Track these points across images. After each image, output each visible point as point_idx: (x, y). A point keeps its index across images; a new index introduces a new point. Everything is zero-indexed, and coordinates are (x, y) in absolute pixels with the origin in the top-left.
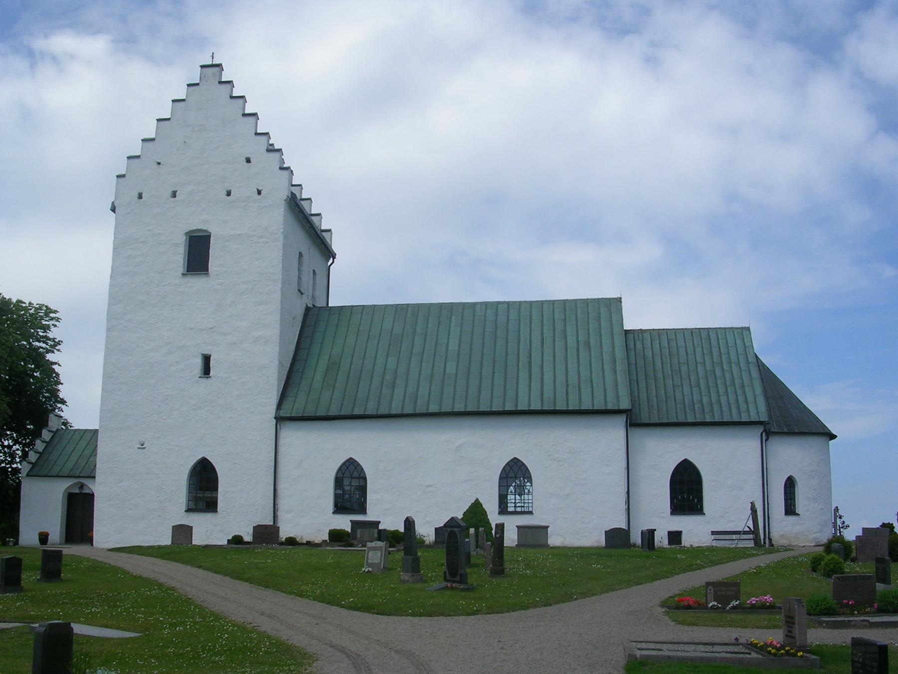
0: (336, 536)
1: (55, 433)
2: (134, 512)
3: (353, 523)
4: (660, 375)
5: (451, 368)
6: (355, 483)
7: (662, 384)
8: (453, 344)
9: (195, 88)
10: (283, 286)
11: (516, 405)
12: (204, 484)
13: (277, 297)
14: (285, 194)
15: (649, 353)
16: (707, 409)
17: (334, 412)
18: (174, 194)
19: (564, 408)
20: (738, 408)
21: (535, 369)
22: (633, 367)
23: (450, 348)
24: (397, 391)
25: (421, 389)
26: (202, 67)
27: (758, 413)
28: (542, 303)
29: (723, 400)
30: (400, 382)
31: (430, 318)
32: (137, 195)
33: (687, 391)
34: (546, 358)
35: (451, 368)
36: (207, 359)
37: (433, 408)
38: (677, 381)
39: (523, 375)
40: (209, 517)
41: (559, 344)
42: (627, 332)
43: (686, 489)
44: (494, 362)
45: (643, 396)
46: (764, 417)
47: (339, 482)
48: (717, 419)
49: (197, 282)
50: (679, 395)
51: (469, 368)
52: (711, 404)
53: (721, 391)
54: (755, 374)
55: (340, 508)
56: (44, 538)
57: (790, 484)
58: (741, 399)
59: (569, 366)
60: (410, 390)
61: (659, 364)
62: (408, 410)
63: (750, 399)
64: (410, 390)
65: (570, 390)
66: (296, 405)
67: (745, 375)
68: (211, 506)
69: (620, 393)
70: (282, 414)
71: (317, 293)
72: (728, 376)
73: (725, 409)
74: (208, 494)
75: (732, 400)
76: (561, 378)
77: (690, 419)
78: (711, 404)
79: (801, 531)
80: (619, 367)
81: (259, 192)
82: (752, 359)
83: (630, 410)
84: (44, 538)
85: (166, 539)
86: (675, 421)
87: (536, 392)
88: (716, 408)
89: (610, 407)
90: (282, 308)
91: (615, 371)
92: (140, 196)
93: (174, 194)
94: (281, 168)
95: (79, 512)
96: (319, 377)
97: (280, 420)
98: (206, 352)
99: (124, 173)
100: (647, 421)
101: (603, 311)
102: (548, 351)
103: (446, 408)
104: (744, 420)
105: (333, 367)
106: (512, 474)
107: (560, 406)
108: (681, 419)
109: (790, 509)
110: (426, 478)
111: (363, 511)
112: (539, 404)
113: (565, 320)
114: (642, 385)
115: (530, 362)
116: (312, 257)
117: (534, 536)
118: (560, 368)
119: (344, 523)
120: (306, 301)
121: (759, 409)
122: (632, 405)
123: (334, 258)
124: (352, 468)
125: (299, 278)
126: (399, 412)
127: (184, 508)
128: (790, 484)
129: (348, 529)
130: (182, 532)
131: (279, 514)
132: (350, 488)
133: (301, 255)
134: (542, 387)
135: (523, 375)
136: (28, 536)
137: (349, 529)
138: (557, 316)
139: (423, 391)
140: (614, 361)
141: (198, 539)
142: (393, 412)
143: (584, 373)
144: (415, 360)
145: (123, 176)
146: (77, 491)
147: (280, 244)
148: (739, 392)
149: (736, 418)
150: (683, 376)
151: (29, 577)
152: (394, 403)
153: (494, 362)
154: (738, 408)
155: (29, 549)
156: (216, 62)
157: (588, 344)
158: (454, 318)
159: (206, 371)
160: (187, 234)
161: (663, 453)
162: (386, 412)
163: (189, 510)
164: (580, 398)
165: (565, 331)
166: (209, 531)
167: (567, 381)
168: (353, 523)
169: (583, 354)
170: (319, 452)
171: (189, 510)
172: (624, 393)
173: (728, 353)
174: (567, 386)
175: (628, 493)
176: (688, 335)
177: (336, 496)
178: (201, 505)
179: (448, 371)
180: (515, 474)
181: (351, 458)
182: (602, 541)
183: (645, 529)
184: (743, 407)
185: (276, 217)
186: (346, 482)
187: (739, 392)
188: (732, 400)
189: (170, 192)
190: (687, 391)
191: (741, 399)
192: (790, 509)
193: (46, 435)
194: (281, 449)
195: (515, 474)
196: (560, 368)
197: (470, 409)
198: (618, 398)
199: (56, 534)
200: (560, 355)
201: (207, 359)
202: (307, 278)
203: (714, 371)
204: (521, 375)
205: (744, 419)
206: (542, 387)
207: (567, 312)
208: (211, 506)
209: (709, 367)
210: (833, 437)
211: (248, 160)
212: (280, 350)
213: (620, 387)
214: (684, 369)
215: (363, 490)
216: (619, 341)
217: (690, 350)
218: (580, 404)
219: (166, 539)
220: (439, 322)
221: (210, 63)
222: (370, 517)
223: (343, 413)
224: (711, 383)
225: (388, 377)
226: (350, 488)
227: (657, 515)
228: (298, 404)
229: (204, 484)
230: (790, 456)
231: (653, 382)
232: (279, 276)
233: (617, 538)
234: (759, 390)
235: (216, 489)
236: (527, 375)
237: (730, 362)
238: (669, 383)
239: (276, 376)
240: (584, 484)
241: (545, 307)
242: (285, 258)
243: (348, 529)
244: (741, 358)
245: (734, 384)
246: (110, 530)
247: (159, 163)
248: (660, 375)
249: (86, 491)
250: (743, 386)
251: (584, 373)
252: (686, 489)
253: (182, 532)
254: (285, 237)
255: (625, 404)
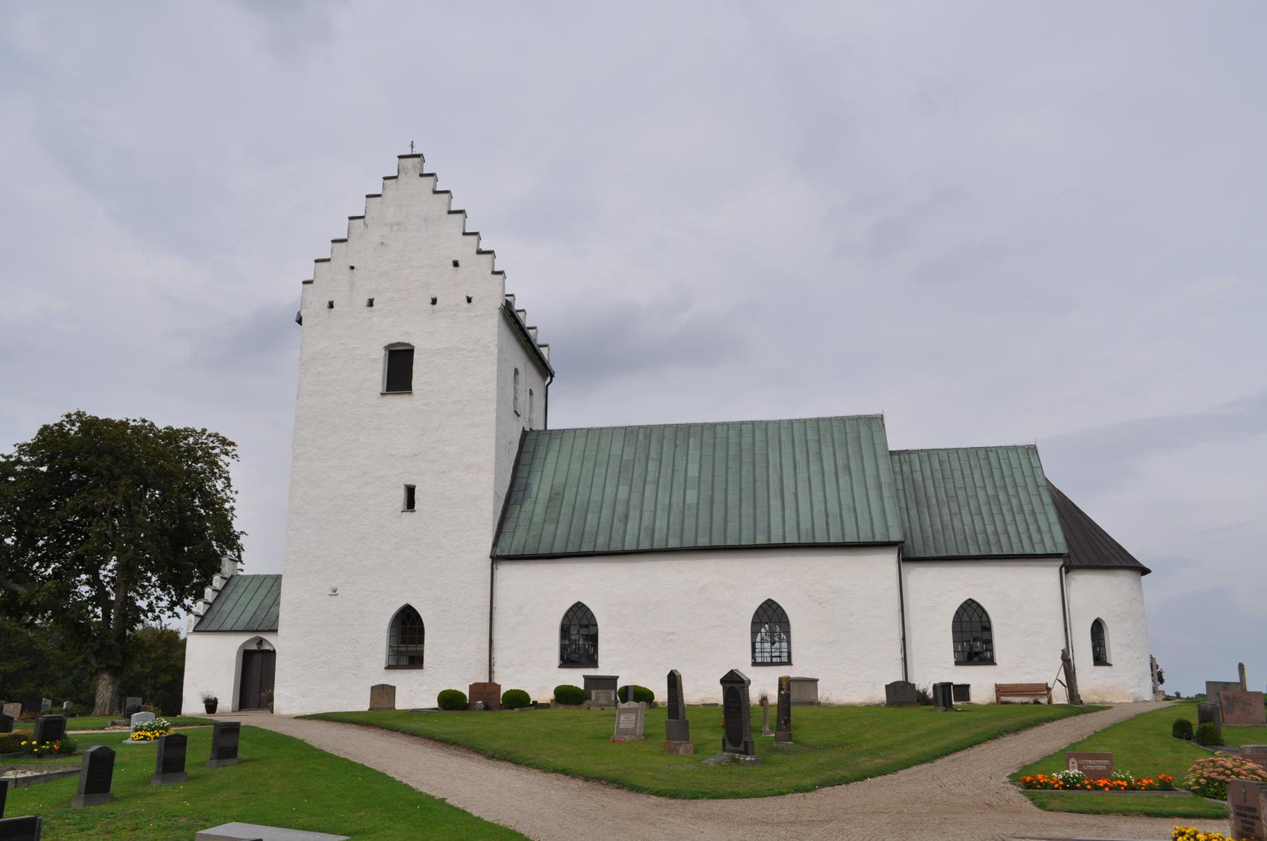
0: (565, 696)
1: (228, 581)
2: (325, 672)
3: (586, 678)
4: (934, 501)
5: (691, 497)
6: (584, 631)
7: (960, 509)
8: (693, 470)
9: (393, 181)
10: (498, 405)
11: (769, 538)
12: (407, 634)
13: (492, 417)
14: (499, 302)
15: (918, 477)
16: (992, 539)
17: (558, 549)
18: (371, 303)
19: (824, 540)
20: (1030, 538)
21: (789, 497)
22: (901, 493)
23: (689, 474)
24: (630, 523)
25: (658, 521)
26: (400, 157)
27: (1055, 544)
28: (791, 422)
29: (1012, 530)
30: (634, 514)
31: (665, 442)
32: (327, 304)
33: (967, 518)
34: (799, 484)
35: (691, 497)
36: (411, 491)
37: (673, 543)
38: (954, 509)
39: (775, 503)
40: (413, 674)
41: (814, 467)
42: (892, 453)
43: (973, 635)
44: (741, 490)
45: (916, 525)
46: (1063, 549)
47: (565, 631)
48: (1006, 551)
49: (398, 402)
50: (957, 525)
51: (712, 496)
52: (996, 533)
53: (1008, 518)
54: (1047, 499)
55: (567, 661)
56: (211, 705)
57: (1098, 628)
58: (1033, 528)
59: (828, 492)
60: (646, 522)
61: (931, 489)
62: (645, 545)
63: (1044, 527)
64: (646, 522)
65: (830, 520)
66: (515, 542)
67: (1035, 500)
68: (416, 661)
69: (890, 523)
70: (498, 552)
71: (535, 415)
72: (1014, 501)
73: (1014, 540)
74: (412, 648)
75: (1022, 529)
76: (819, 506)
77: (973, 552)
78: (996, 533)
79: (1119, 684)
80: (886, 493)
81: (469, 300)
82: (1041, 482)
83: (903, 542)
84: (211, 705)
85: (363, 704)
86: (955, 554)
87: (791, 522)
88: (1003, 538)
89: (878, 539)
90: (497, 431)
91: (881, 498)
92: (331, 305)
93: (371, 303)
94: (494, 273)
95: (256, 673)
96: (540, 510)
97: (496, 559)
98: (410, 483)
99: (311, 278)
100: (923, 555)
101: (864, 430)
102: (802, 476)
103: (688, 543)
104: (1049, 552)
105: (556, 497)
106: (765, 619)
107: (821, 538)
108: (963, 552)
109: (1100, 658)
110: (676, 627)
111: (593, 662)
112: (796, 536)
113: (819, 441)
114: (913, 513)
115: (782, 489)
116: (529, 375)
117: (795, 693)
118: (818, 494)
119: (575, 678)
120: (522, 424)
121: (1056, 540)
122: (905, 536)
123: (552, 376)
124: (580, 614)
125: (515, 398)
126: (633, 547)
127: (384, 664)
128: (1098, 628)
129: (581, 685)
130: (383, 693)
131: (496, 669)
132: (579, 636)
133: (516, 372)
134: (798, 517)
135: (775, 503)
136: (192, 705)
137: (582, 687)
138: (810, 437)
139: (661, 524)
140: (880, 486)
141: (401, 704)
142: (627, 548)
143: (846, 501)
144: (649, 488)
145: (310, 282)
146: (254, 647)
147: (494, 358)
148: (1030, 519)
149: (1028, 551)
150: (961, 502)
151: (198, 754)
152: (627, 538)
153: (741, 490)
154: (1030, 538)
155: (193, 721)
156: (416, 152)
157: (848, 468)
158: (691, 440)
159: (410, 504)
160: (386, 348)
161: (941, 590)
162: (619, 549)
163: (389, 667)
164: (843, 530)
165: (820, 453)
166: (416, 692)
167: (826, 510)
168: (586, 678)
169: (843, 479)
170: (544, 592)
171: (389, 667)
172: (893, 521)
173: (1013, 476)
174: (827, 516)
175: (904, 639)
176: (982, 454)
177: (563, 648)
178: (404, 661)
179: (688, 501)
180: (770, 619)
181: (579, 603)
182: (881, 696)
183: (937, 682)
184: (1036, 537)
185: (492, 327)
186: (573, 631)
187: (1030, 519)
188: (1022, 529)
189: (366, 302)
190: (967, 518)
191: (1033, 528)
192: (1100, 658)
193: (217, 581)
194: (497, 585)
195: (770, 619)
196: (818, 494)
197: (716, 543)
198: (887, 528)
199: (227, 702)
200: (816, 480)
201: (411, 491)
202: (523, 397)
203: (997, 495)
204: (772, 503)
205: (1039, 551)
206: (798, 517)
207: (822, 432)
208: (416, 661)
209: (991, 492)
210: (1145, 571)
211: (456, 264)
212: (496, 478)
213: (889, 517)
214: (961, 494)
215: (593, 639)
216: (883, 463)
217: (967, 472)
218: (843, 536)
219: (363, 704)
220: (676, 446)
221: (409, 153)
222: (603, 670)
223: (570, 550)
224: (995, 510)
225: (620, 509)
226: (579, 636)
227: (935, 665)
228: (519, 540)
229: (407, 634)
230: (1095, 592)
231: (925, 509)
232: (493, 395)
233: (901, 693)
234: (1053, 517)
235: (422, 641)
236: (780, 505)
237: (1016, 486)
238: (945, 510)
239: (491, 508)
240: (861, 631)
241: (796, 427)
242: (500, 374)
243: (581, 685)
244: (1008, 480)
245: (1022, 510)
246: (293, 696)
247: (352, 268)
248: (934, 501)
249: (267, 647)
250: (1033, 513)
251: (846, 501)
252: (973, 635)
253: (383, 693)
254: (500, 351)
255: (896, 536)
